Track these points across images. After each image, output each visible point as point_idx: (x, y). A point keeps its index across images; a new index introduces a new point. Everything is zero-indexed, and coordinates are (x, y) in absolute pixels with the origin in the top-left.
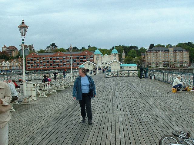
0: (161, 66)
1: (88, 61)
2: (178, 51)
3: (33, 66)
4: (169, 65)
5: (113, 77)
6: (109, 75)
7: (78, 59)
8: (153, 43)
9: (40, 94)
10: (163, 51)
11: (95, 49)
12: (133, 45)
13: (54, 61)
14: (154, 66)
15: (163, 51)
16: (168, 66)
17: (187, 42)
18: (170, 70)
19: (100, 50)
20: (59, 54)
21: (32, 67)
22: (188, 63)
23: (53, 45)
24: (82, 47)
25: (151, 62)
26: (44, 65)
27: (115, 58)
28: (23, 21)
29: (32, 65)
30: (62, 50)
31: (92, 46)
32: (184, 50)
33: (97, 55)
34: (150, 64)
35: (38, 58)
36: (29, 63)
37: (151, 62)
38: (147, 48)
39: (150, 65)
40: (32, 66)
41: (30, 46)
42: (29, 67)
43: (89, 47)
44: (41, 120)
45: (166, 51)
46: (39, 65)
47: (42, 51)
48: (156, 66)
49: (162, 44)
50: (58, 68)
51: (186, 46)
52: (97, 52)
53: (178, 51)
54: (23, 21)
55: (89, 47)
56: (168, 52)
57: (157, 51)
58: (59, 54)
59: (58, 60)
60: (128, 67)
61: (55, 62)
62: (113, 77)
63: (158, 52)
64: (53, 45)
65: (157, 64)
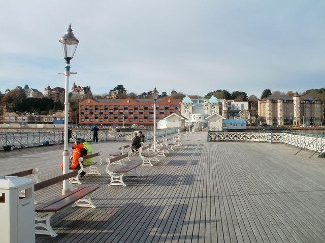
1: (174, 114)
3: (114, 113)
5: (220, 141)
9: (112, 179)
11: (181, 97)
12: (240, 90)
13: (121, 111)
17: (319, 88)
19: (189, 96)
23: (120, 88)
27: (213, 109)
28: (70, 26)
30: (133, 96)
31: (178, 91)
33: (187, 105)
43: (173, 92)
45: (289, 101)
46: (117, 117)
48: (171, 139)
51: (321, 91)
52: (186, 100)
54: (70, 26)
55: (173, 92)
58: (128, 101)
60: (233, 124)
62: (220, 141)
64: (120, 88)
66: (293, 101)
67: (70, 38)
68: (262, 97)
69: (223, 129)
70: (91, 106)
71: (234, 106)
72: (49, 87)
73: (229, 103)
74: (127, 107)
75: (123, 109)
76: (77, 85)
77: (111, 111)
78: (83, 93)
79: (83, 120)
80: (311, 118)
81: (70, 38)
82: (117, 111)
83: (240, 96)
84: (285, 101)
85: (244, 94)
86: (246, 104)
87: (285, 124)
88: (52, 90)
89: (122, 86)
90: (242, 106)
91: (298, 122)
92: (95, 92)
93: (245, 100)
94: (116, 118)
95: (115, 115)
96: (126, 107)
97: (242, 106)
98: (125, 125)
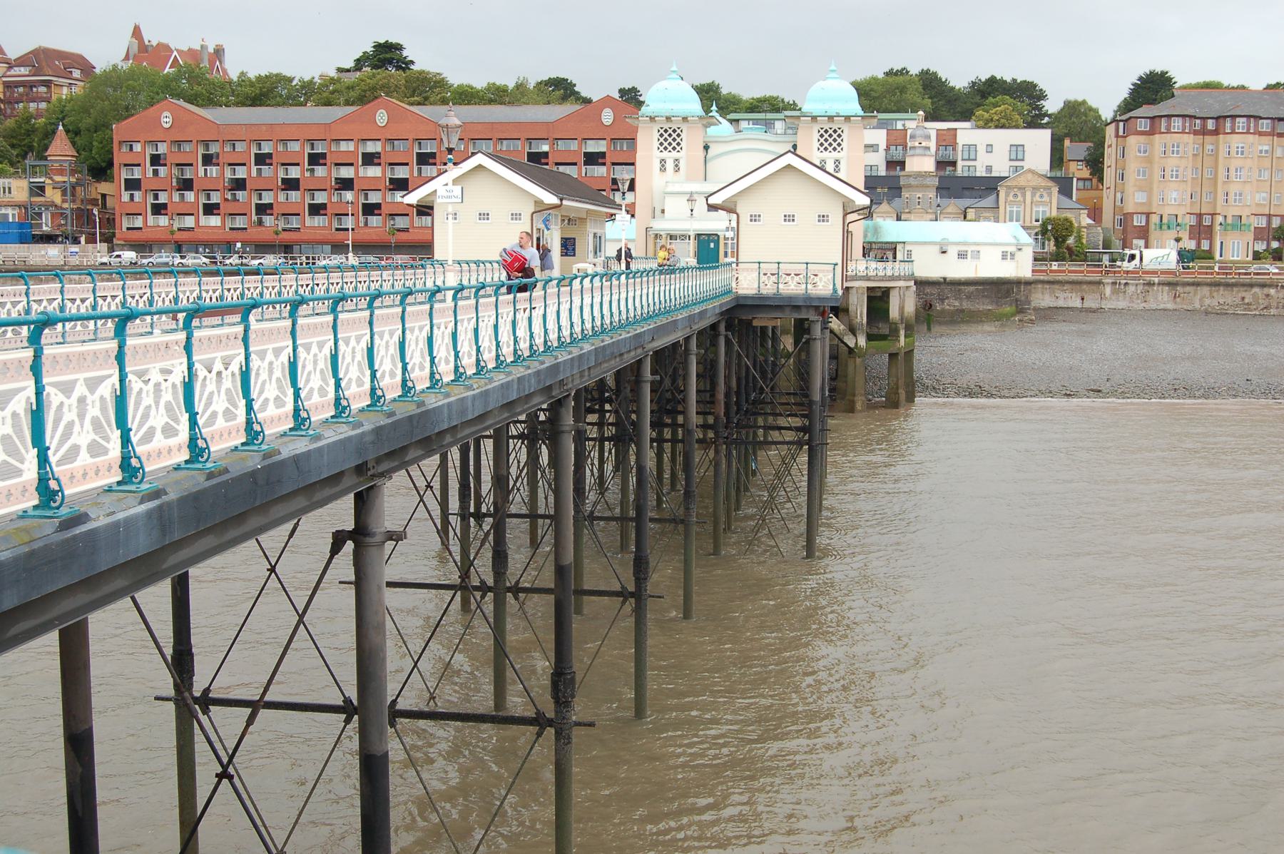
0: (1235, 249)
2: (1241, 122)
8: (1143, 68)
10: (1265, 125)
13: (346, 173)
14: (1160, 255)
15: (1265, 125)
18: (136, 273)
20: (382, 118)
21: (268, 220)
23: (386, 55)
25: (1148, 215)
26: (370, 209)
27: (670, 156)
35: (266, 148)
37: (1148, 215)
38: (1107, 102)
40: (370, 209)
42: (138, 222)
46: (323, 206)
49: (1273, 82)
50: (365, 235)
55: (142, 49)
57: (1211, 125)
58: (382, 118)
59: (374, 172)
60: (953, 251)
61: (346, 184)
63: (1216, 132)
64: (386, 55)
68: (1128, 106)
73: (947, 140)
76: (152, 37)
83: (1007, 100)
85: (1028, 93)
86: (1038, 143)
87: (1257, 256)
89: (398, 47)
90: (1017, 152)
95: (259, 192)
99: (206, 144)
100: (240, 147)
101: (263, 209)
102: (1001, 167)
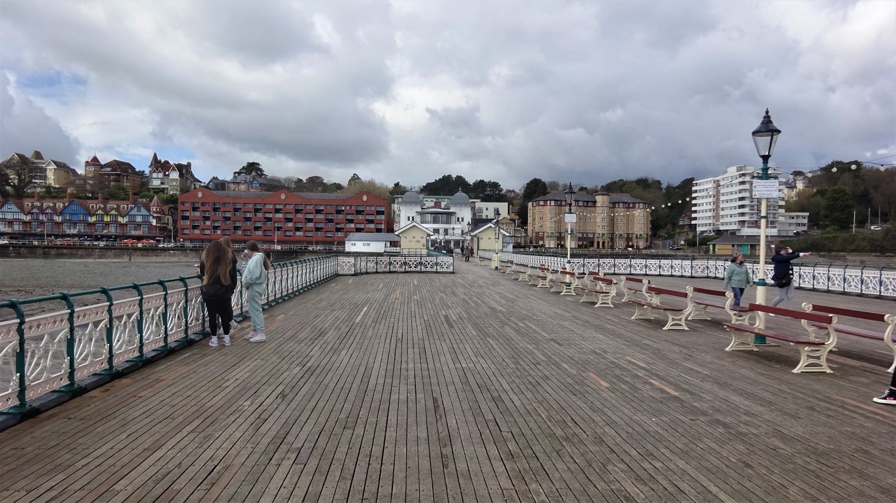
4: (595, 245)
6: (622, 268)
7: (360, 217)
16: (593, 246)
20: (283, 196)
22: (647, 239)
24: (38, 155)
28: (767, 112)
29: (238, 224)
31: (104, 159)
32: (638, 200)
34: (542, 239)
36: (185, 218)
39: (541, 243)
41: (180, 167)
44: (352, 338)
45: (588, 202)
47: (219, 185)
53: (621, 205)
54: (767, 112)
56: (595, 206)
58: (283, 196)
65: (629, 239)
66: (595, 202)
67: (767, 128)
69: (759, 201)
70: (203, 204)
71: (481, 210)
72: (95, 159)
74: (281, 207)
75: (293, 211)
77: (248, 215)
78: (175, 175)
79: (187, 232)
80: (628, 234)
81: (767, 128)
82: (260, 215)
84: (581, 204)
88: (102, 167)
89: (258, 164)
90: (497, 213)
91: (604, 242)
92: (203, 173)
93: (501, 198)
94: (257, 229)
96: (278, 207)
97: (497, 213)
98: (279, 242)
99: (193, 203)
100: (186, 205)
101: (236, 228)
102: (491, 215)
